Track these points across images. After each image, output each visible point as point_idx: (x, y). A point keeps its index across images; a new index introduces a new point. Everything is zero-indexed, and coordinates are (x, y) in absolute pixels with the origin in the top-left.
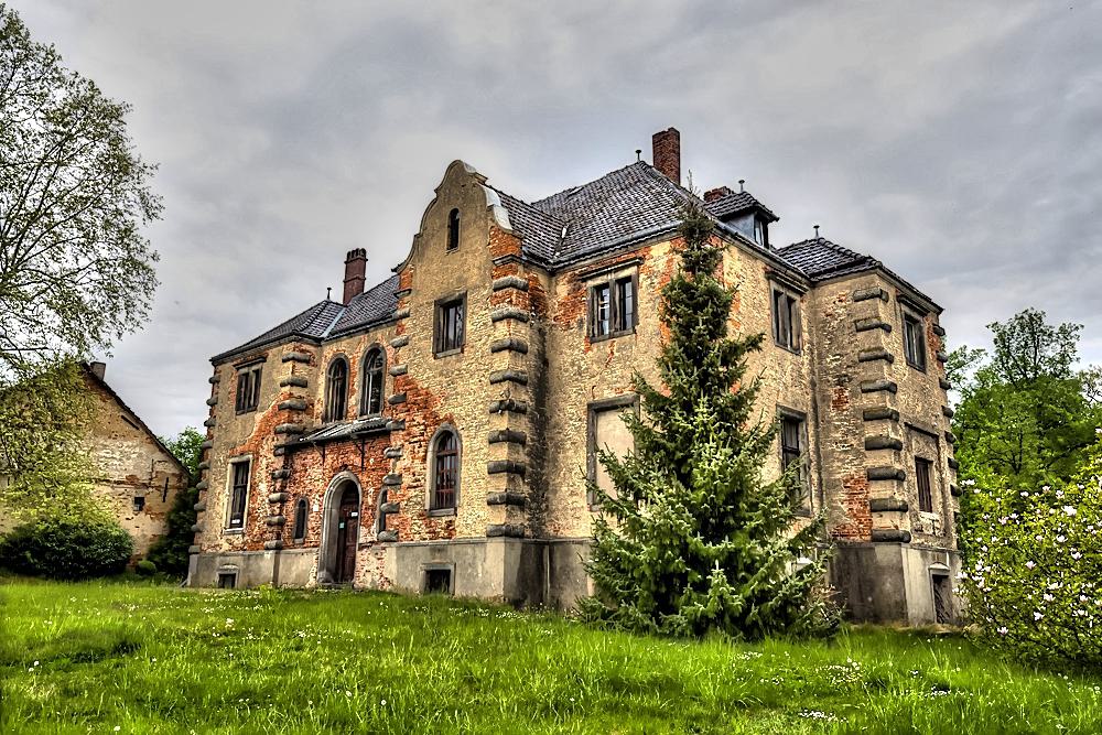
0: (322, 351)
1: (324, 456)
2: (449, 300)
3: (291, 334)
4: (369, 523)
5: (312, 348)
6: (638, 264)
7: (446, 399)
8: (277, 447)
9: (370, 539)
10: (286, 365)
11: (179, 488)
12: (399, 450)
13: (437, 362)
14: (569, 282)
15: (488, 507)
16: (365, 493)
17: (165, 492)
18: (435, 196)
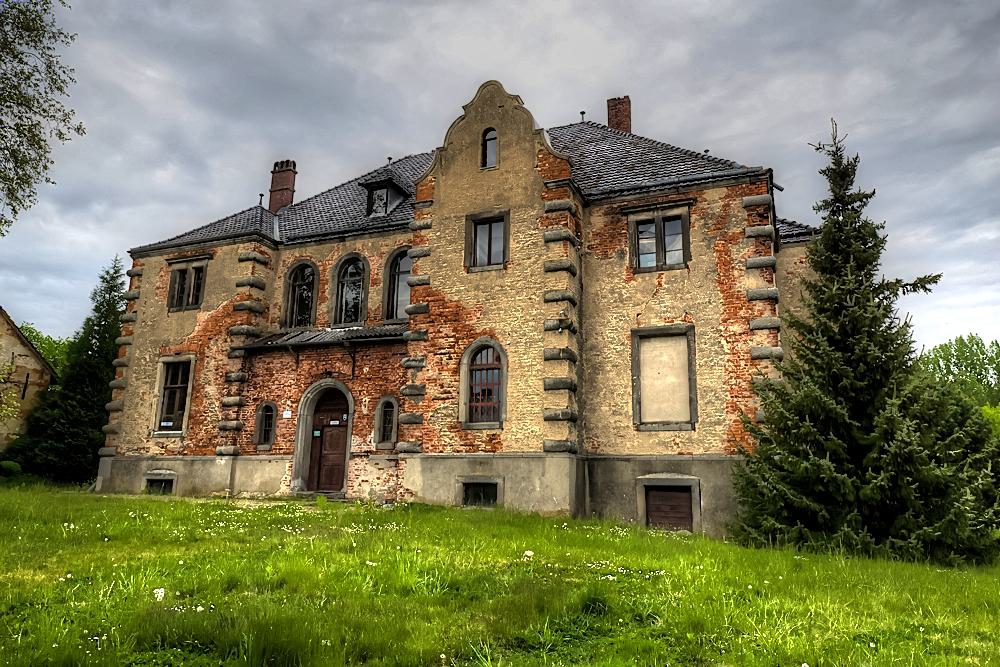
0: (279, 256)
1: (297, 362)
2: (485, 216)
4: (364, 432)
5: (269, 251)
6: (690, 205)
7: (485, 314)
8: (234, 349)
9: (365, 448)
10: (243, 264)
11: (39, 385)
12: (422, 360)
13: (472, 276)
14: (606, 214)
16: (358, 402)
17: (24, 391)
18: (462, 112)
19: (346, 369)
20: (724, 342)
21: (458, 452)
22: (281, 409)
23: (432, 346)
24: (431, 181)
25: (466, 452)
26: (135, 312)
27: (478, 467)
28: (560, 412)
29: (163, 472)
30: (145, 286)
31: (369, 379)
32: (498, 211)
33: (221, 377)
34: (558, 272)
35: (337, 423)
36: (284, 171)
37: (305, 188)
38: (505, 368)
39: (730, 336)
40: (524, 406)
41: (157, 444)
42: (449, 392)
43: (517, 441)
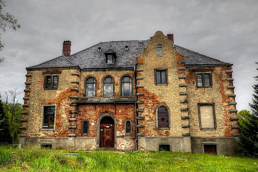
1: (95, 108)
3: (76, 67)
4: (121, 130)
6: (212, 71)
9: (122, 135)
12: (143, 110)
13: (157, 86)
15: (182, 128)
19: (113, 111)
20: (222, 108)
21: (157, 136)
22: (91, 122)
23: (146, 106)
24: (142, 57)
25: (159, 136)
26: (30, 89)
27: (163, 140)
28: (187, 125)
29: (47, 142)
30: (33, 81)
31: (121, 114)
32: (164, 68)
33: (68, 112)
34: (183, 87)
35: (109, 127)
36: (67, 45)
37: (74, 50)
38: (170, 113)
39: (224, 106)
40: (176, 124)
41: (43, 133)
42: (152, 119)
43: (174, 133)
